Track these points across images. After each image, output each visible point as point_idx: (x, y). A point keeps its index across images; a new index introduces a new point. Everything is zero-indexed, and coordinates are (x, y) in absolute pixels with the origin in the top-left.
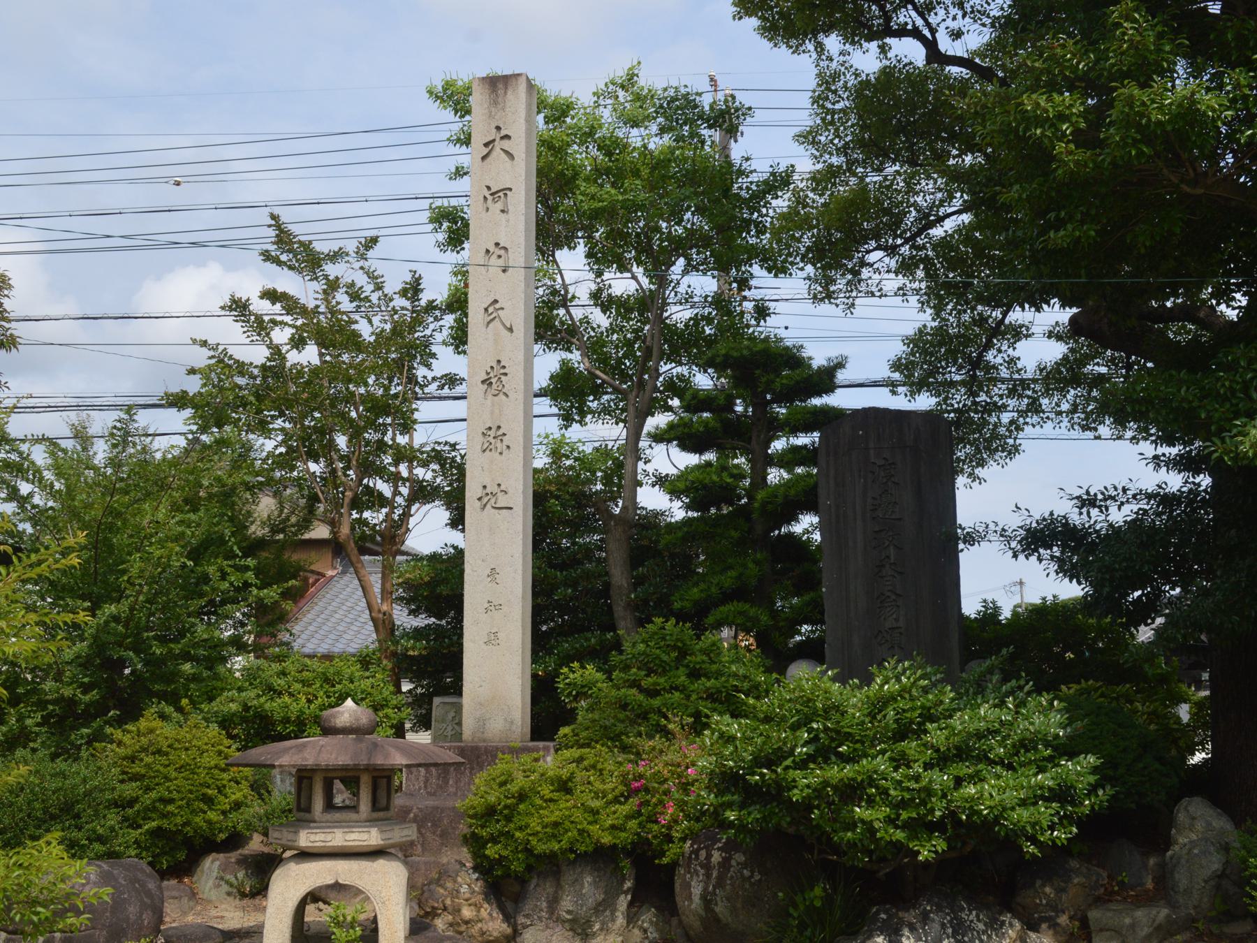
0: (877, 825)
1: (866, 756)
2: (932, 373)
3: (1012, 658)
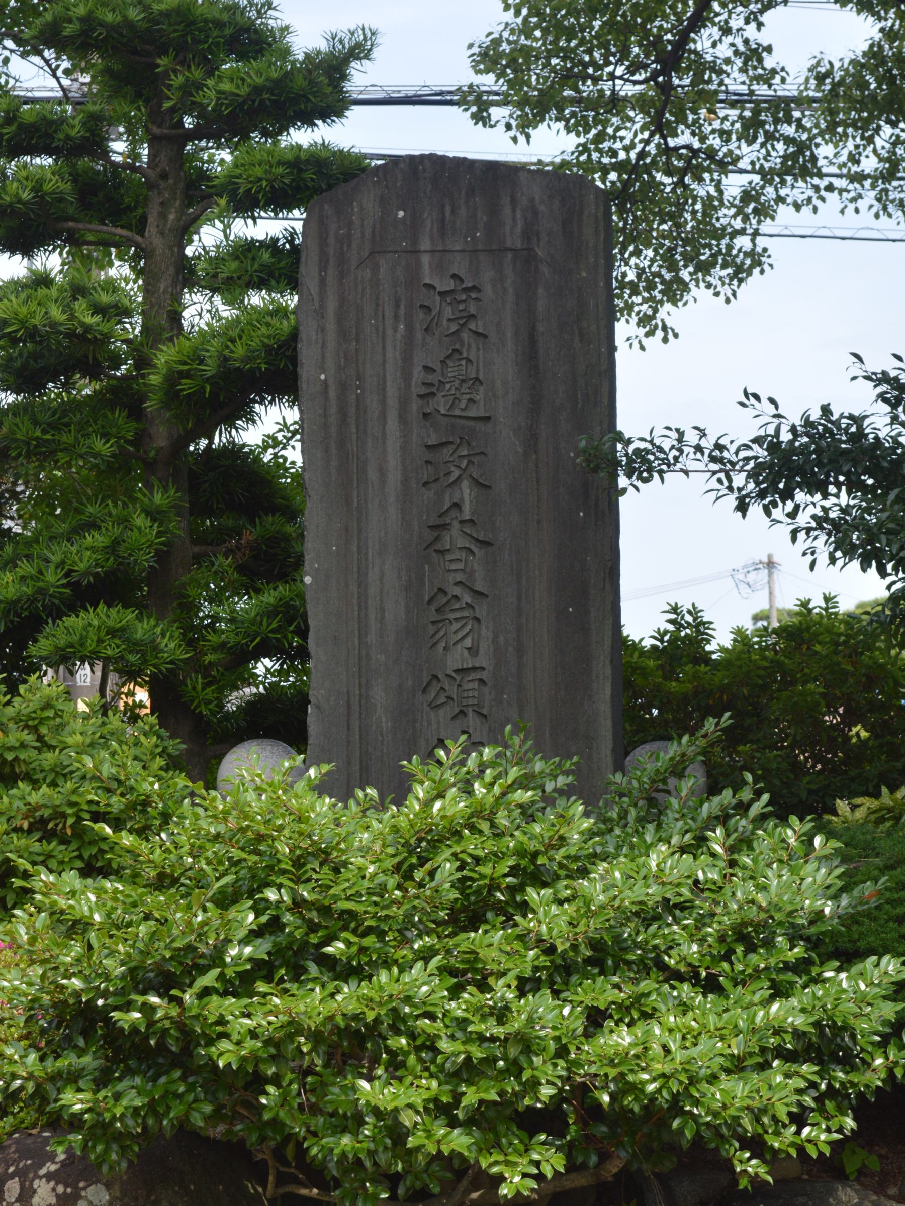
0: (407, 1119)
1: (387, 964)
2: (568, 78)
3: (731, 737)
